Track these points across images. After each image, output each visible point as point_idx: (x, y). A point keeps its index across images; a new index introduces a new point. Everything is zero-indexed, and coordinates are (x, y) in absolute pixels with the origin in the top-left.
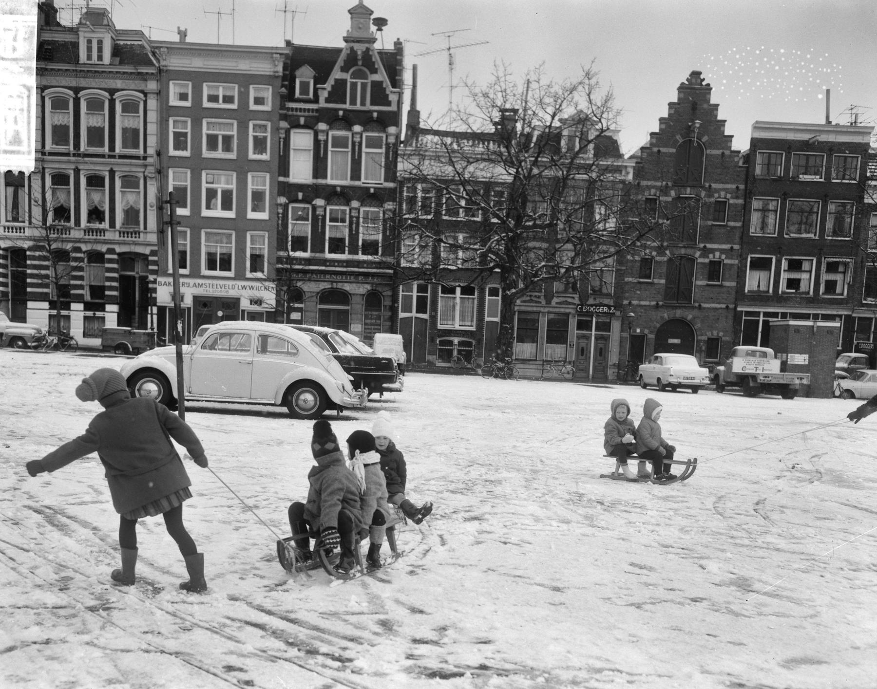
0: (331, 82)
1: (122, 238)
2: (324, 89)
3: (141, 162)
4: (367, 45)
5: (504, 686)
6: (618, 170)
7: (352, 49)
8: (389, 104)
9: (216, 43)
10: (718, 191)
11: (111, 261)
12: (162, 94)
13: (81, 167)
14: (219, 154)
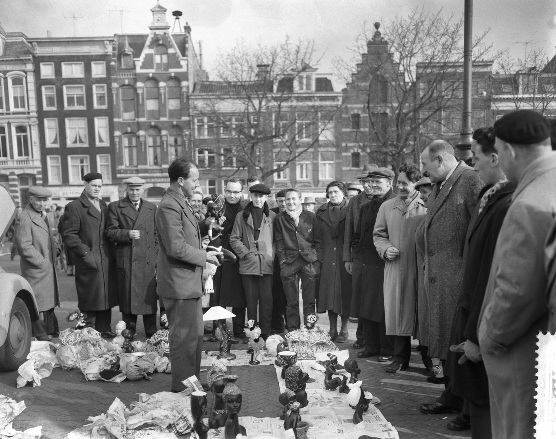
0: (143, 56)
1: (18, 165)
2: (139, 61)
3: (27, 115)
4: (164, 31)
5: (359, 383)
6: (333, 98)
7: (155, 34)
8: (181, 67)
9: (46, 37)
10: (353, 109)
11: (14, 180)
12: (37, 72)
13: (11, 121)
14: (77, 107)
